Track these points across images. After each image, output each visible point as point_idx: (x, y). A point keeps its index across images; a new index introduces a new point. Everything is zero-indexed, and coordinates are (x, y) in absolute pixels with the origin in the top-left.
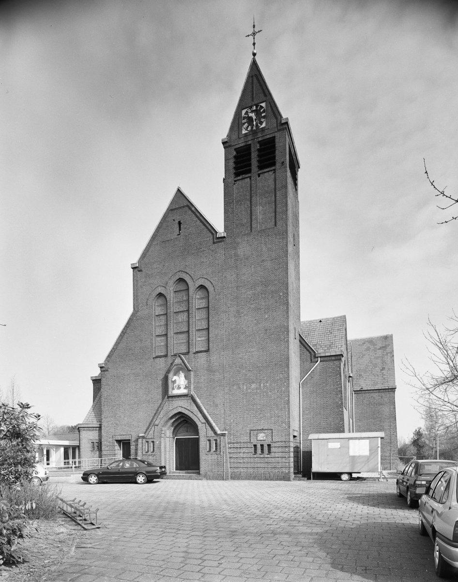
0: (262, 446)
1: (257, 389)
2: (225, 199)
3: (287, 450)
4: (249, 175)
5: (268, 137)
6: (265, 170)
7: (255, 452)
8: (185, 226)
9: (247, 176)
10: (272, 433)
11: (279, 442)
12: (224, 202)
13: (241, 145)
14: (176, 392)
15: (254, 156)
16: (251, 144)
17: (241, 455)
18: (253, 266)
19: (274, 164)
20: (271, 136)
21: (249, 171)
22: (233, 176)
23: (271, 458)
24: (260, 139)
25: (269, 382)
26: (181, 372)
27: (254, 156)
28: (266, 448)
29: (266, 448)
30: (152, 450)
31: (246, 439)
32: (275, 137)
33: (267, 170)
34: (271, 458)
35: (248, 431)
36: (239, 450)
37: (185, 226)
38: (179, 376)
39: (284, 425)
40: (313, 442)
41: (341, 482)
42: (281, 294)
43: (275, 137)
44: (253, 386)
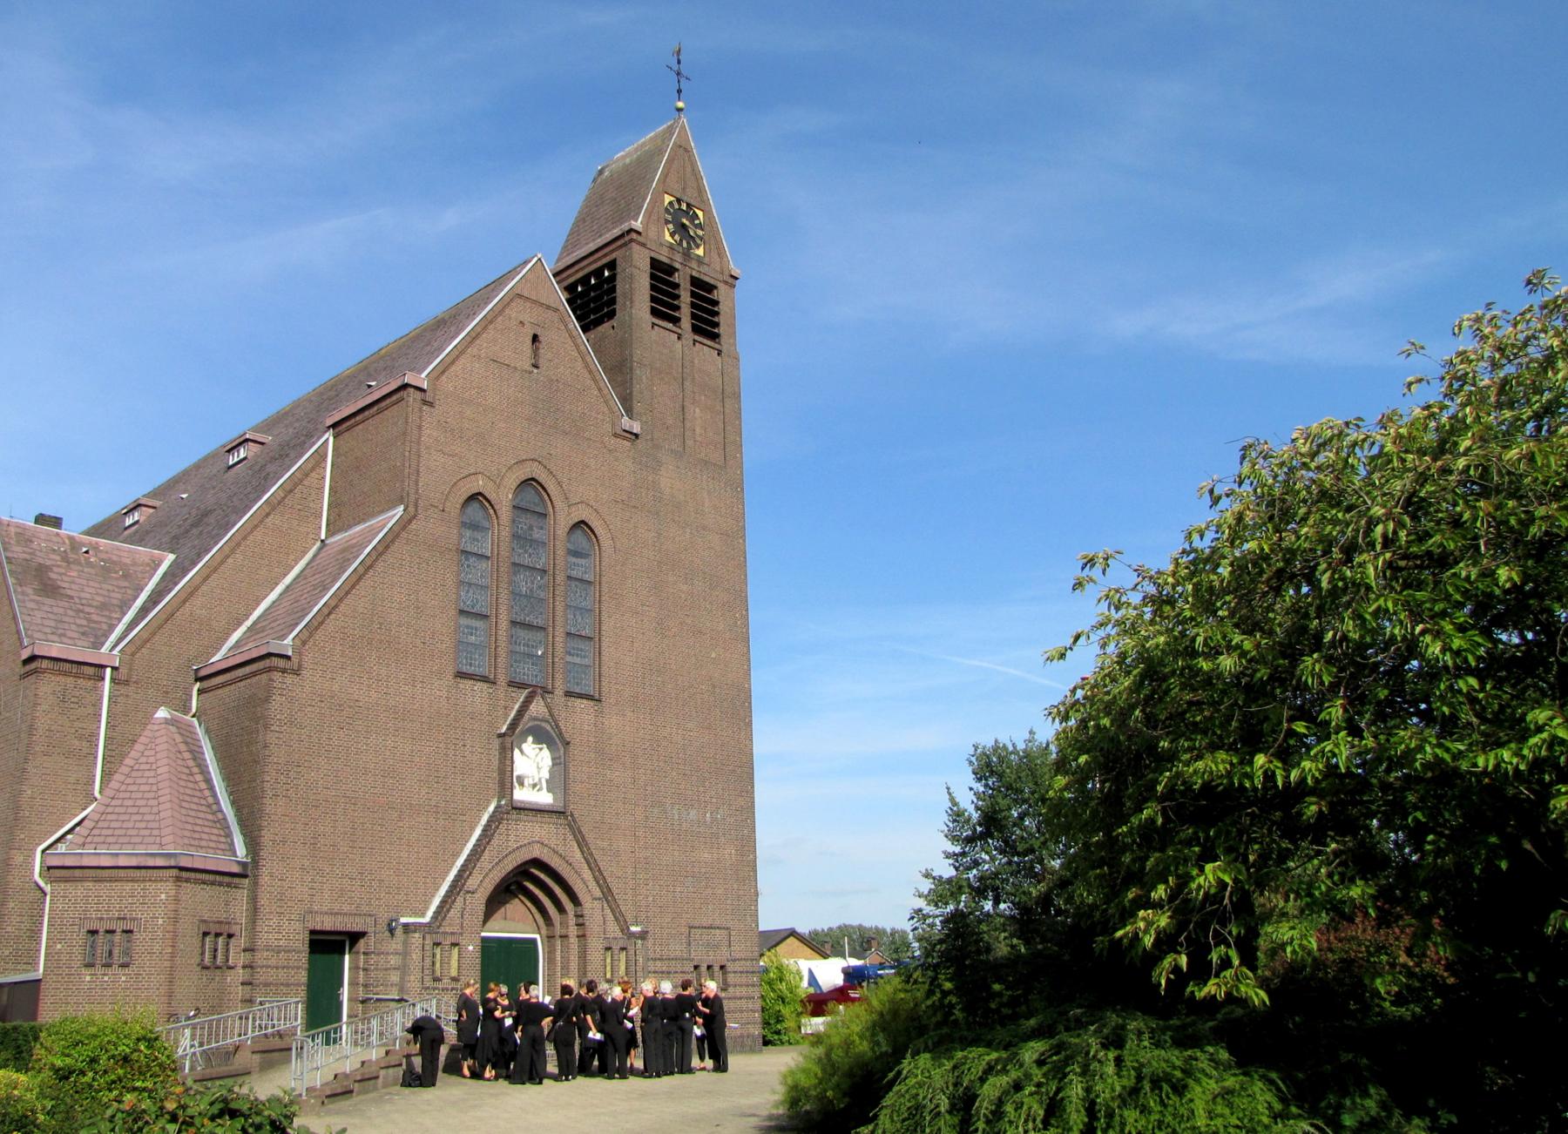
5: (707, 279)
16: (677, 270)
20: (712, 282)
25: (721, 811)
35: (685, 930)
44: (693, 814)
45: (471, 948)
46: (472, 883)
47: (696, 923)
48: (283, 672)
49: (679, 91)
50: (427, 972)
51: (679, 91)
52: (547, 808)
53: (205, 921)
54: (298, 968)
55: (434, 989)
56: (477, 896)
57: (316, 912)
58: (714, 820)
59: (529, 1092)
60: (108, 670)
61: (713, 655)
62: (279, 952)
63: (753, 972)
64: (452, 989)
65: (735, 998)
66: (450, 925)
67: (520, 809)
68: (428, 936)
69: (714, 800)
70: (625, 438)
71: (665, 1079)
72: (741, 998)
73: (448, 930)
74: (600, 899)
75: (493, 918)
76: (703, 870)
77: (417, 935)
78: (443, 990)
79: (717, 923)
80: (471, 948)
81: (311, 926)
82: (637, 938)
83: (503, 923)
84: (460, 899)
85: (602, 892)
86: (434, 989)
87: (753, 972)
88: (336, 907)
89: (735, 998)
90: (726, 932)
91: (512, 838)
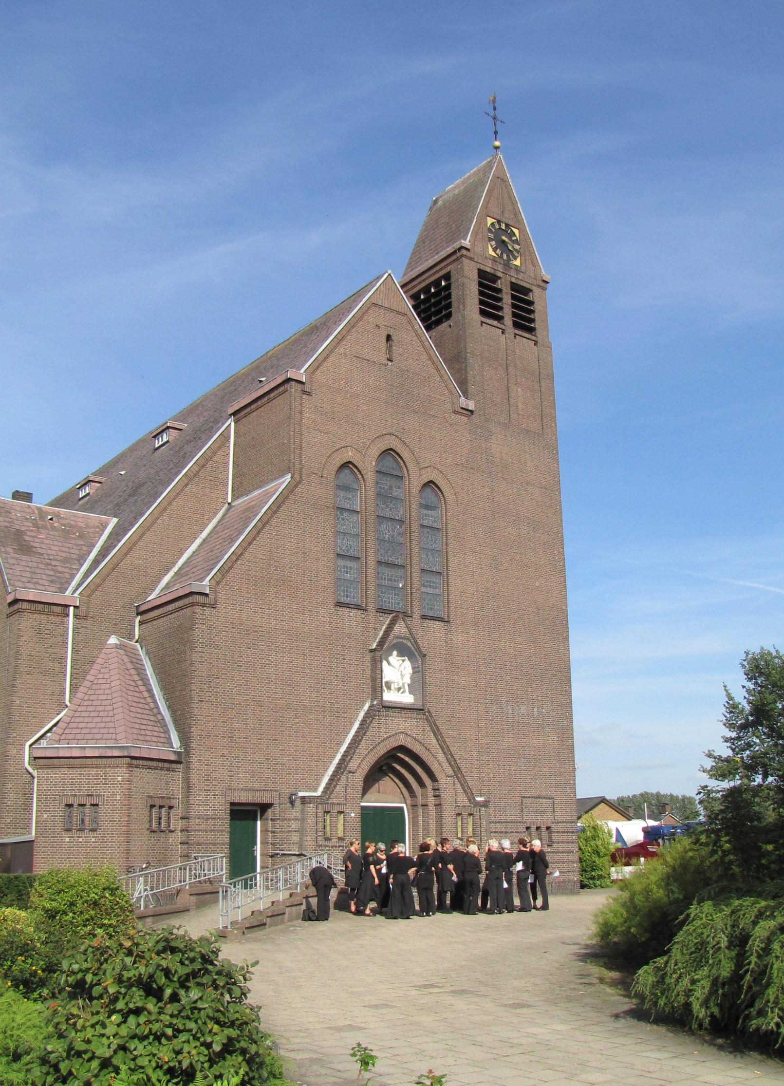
16: (500, 278)
20: (528, 286)
23: (553, 852)
35: (519, 800)
43: (531, 291)
44: (523, 709)
47: (527, 794)
49: (496, 133)
51: (496, 133)
53: (151, 797)
54: (222, 831)
55: (326, 846)
60: (72, 609)
62: (207, 819)
69: (540, 698)
70: (462, 414)
72: (563, 852)
79: (544, 794)
81: (230, 799)
83: (377, 795)
86: (326, 846)
89: (558, 852)
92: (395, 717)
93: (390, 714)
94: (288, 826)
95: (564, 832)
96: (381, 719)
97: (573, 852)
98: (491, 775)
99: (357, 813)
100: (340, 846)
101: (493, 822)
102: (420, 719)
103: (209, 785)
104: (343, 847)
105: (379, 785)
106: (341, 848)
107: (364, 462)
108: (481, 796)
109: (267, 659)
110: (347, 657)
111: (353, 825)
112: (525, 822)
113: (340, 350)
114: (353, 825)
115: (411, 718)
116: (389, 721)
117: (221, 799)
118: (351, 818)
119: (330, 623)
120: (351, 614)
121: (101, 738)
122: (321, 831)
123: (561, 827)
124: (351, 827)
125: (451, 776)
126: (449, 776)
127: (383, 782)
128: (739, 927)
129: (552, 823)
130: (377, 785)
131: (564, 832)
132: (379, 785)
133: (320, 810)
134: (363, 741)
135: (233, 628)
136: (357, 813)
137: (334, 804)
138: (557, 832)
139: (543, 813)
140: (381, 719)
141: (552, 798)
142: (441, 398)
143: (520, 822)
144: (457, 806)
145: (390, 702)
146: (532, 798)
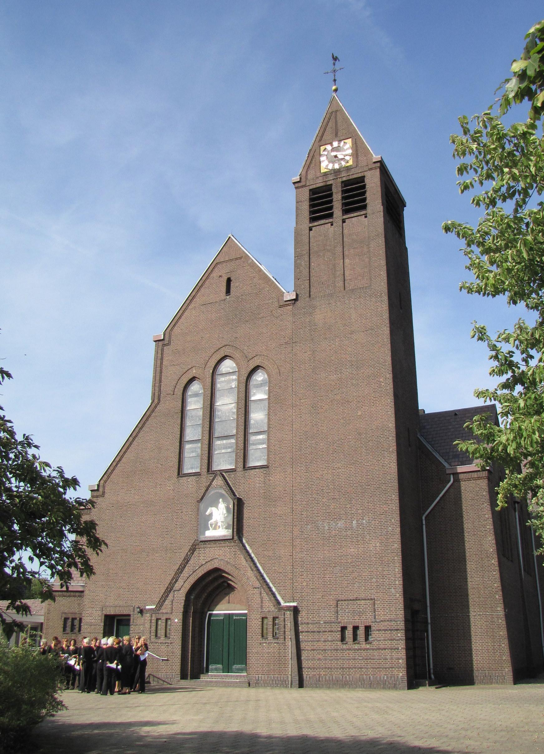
0: (355, 638)
1: (346, 529)
2: (295, 249)
3: (399, 635)
4: (331, 220)
5: (355, 176)
6: (352, 215)
7: (343, 639)
8: (237, 284)
9: (327, 221)
10: (374, 604)
11: (385, 621)
12: (295, 254)
13: (318, 185)
14: (210, 534)
15: (337, 197)
16: (331, 185)
17: (321, 645)
18: (337, 340)
19: (364, 207)
20: (360, 175)
21: (331, 215)
22: (307, 220)
23: (373, 649)
24: (344, 179)
25: (366, 518)
26: (221, 500)
27: (337, 197)
28: (361, 632)
29: (361, 632)
30: (160, 622)
31: (327, 615)
32: (364, 177)
33: (355, 214)
34: (373, 649)
35: (333, 603)
36: (316, 636)
37: (237, 284)
38: (217, 508)
39: (393, 590)
40: (446, 470)
41: (536, 52)
42: (381, 380)
43: (364, 177)
44: (341, 524)
45: (176, 620)
46: (177, 586)
47: (343, 597)
48: (97, 497)
49: (335, 80)
50: (152, 634)
51: (335, 80)
52: (221, 538)
53: (66, 613)
54: (99, 633)
55: (156, 643)
56: (181, 592)
57: (107, 606)
58: (358, 525)
59: (109, 697)
60: (452, 476)
61: (359, 413)
62: (91, 626)
63: (397, 630)
64: (166, 643)
65: (379, 649)
66: (165, 608)
67: (205, 541)
68: (154, 615)
69: (360, 511)
70: (288, 305)
71: (93, 696)
72: (385, 649)
73: (164, 611)
74: (258, 588)
75: (221, 602)
76: (349, 561)
77: (148, 615)
78: (161, 643)
79: (363, 596)
80: (176, 620)
81: (105, 612)
82: (286, 610)
83: (227, 605)
84: (171, 595)
85: (260, 583)
86: (156, 643)
87: (397, 630)
88: (116, 603)
89: (379, 649)
90: (371, 602)
91: (202, 558)
92: (212, 548)
93: (212, 545)
94: (138, 629)
95: (387, 630)
96: (201, 550)
97: (398, 649)
98: (305, 584)
99: (180, 619)
100: (166, 643)
101: (305, 623)
102: (232, 546)
103: (94, 604)
104: (168, 643)
105: (229, 597)
106: (167, 644)
107: (204, 374)
108: (294, 602)
109: (131, 522)
110: (184, 510)
111: (176, 627)
112: (340, 622)
113: (192, 305)
114: (176, 627)
115: (225, 547)
116: (207, 550)
117: (100, 613)
118: (175, 622)
119: (173, 490)
120: (189, 480)
121: (77, 578)
122: (153, 632)
123: (382, 626)
124: (175, 629)
125: (258, 588)
126: (256, 588)
127: (233, 596)
128: (27, 708)
129: (372, 622)
130: (227, 598)
131: (387, 630)
132: (229, 597)
133: (154, 618)
134: (186, 567)
135: (113, 506)
136: (180, 619)
137: (163, 613)
138: (377, 630)
139: (360, 614)
140: (201, 550)
141: (371, 599)
142: (269, 301)
143: (334, 623)
144: (262, 612)
145: (210, 537)
146: (348, 600)
